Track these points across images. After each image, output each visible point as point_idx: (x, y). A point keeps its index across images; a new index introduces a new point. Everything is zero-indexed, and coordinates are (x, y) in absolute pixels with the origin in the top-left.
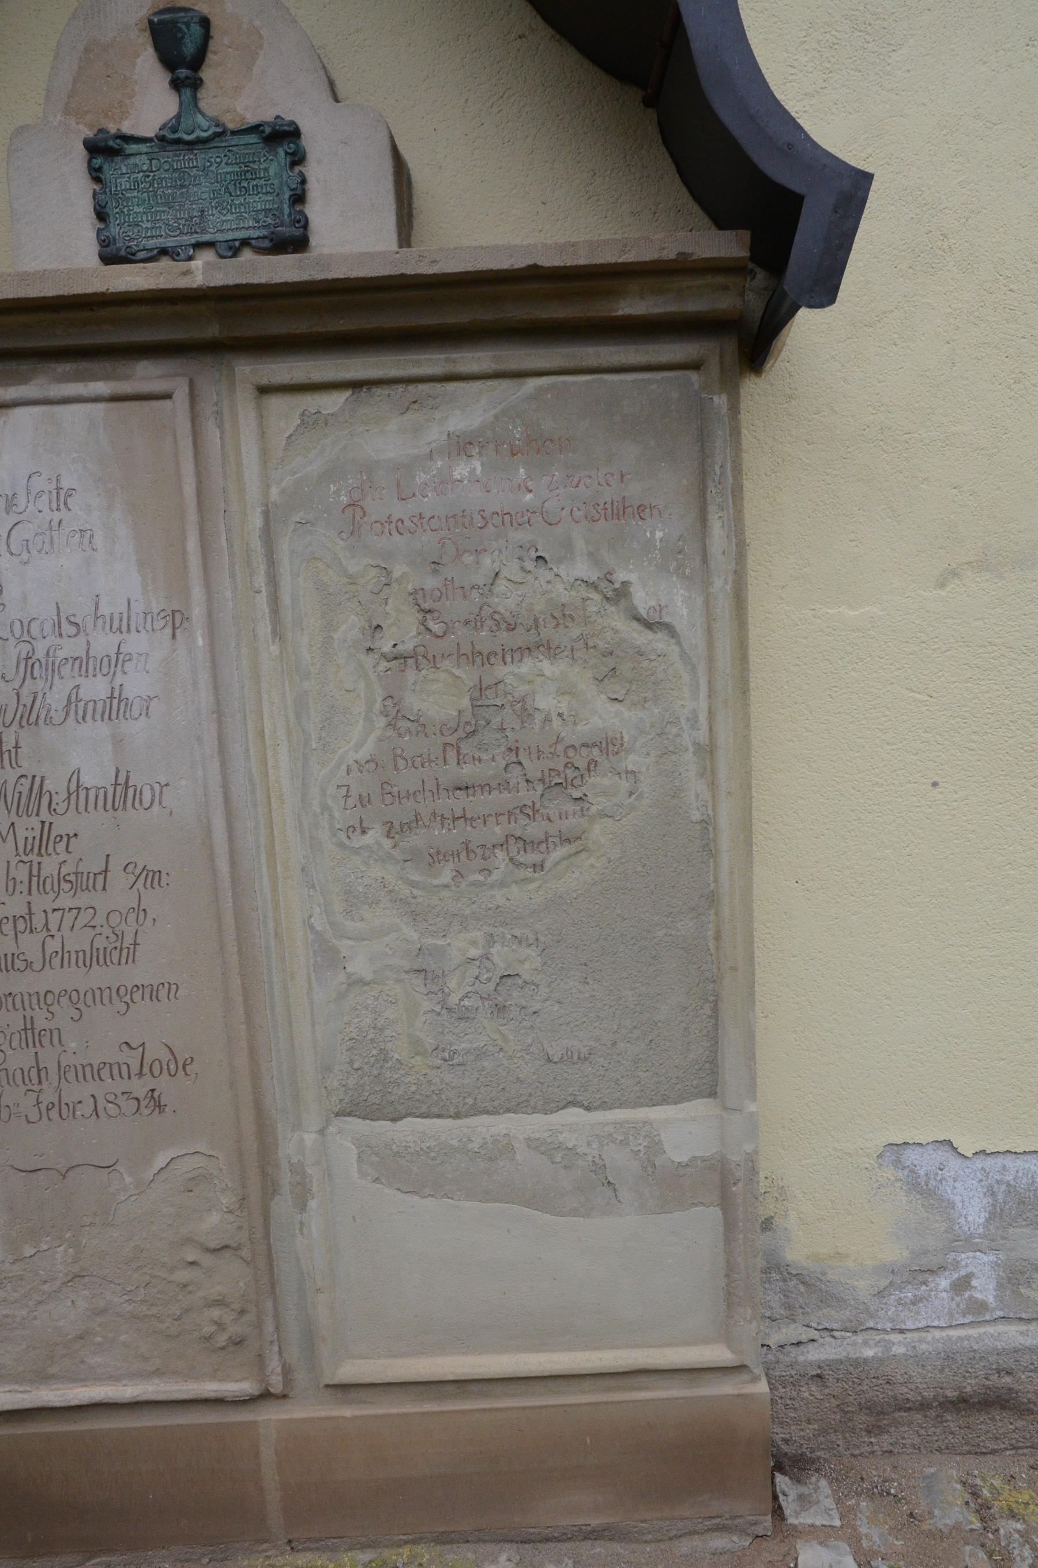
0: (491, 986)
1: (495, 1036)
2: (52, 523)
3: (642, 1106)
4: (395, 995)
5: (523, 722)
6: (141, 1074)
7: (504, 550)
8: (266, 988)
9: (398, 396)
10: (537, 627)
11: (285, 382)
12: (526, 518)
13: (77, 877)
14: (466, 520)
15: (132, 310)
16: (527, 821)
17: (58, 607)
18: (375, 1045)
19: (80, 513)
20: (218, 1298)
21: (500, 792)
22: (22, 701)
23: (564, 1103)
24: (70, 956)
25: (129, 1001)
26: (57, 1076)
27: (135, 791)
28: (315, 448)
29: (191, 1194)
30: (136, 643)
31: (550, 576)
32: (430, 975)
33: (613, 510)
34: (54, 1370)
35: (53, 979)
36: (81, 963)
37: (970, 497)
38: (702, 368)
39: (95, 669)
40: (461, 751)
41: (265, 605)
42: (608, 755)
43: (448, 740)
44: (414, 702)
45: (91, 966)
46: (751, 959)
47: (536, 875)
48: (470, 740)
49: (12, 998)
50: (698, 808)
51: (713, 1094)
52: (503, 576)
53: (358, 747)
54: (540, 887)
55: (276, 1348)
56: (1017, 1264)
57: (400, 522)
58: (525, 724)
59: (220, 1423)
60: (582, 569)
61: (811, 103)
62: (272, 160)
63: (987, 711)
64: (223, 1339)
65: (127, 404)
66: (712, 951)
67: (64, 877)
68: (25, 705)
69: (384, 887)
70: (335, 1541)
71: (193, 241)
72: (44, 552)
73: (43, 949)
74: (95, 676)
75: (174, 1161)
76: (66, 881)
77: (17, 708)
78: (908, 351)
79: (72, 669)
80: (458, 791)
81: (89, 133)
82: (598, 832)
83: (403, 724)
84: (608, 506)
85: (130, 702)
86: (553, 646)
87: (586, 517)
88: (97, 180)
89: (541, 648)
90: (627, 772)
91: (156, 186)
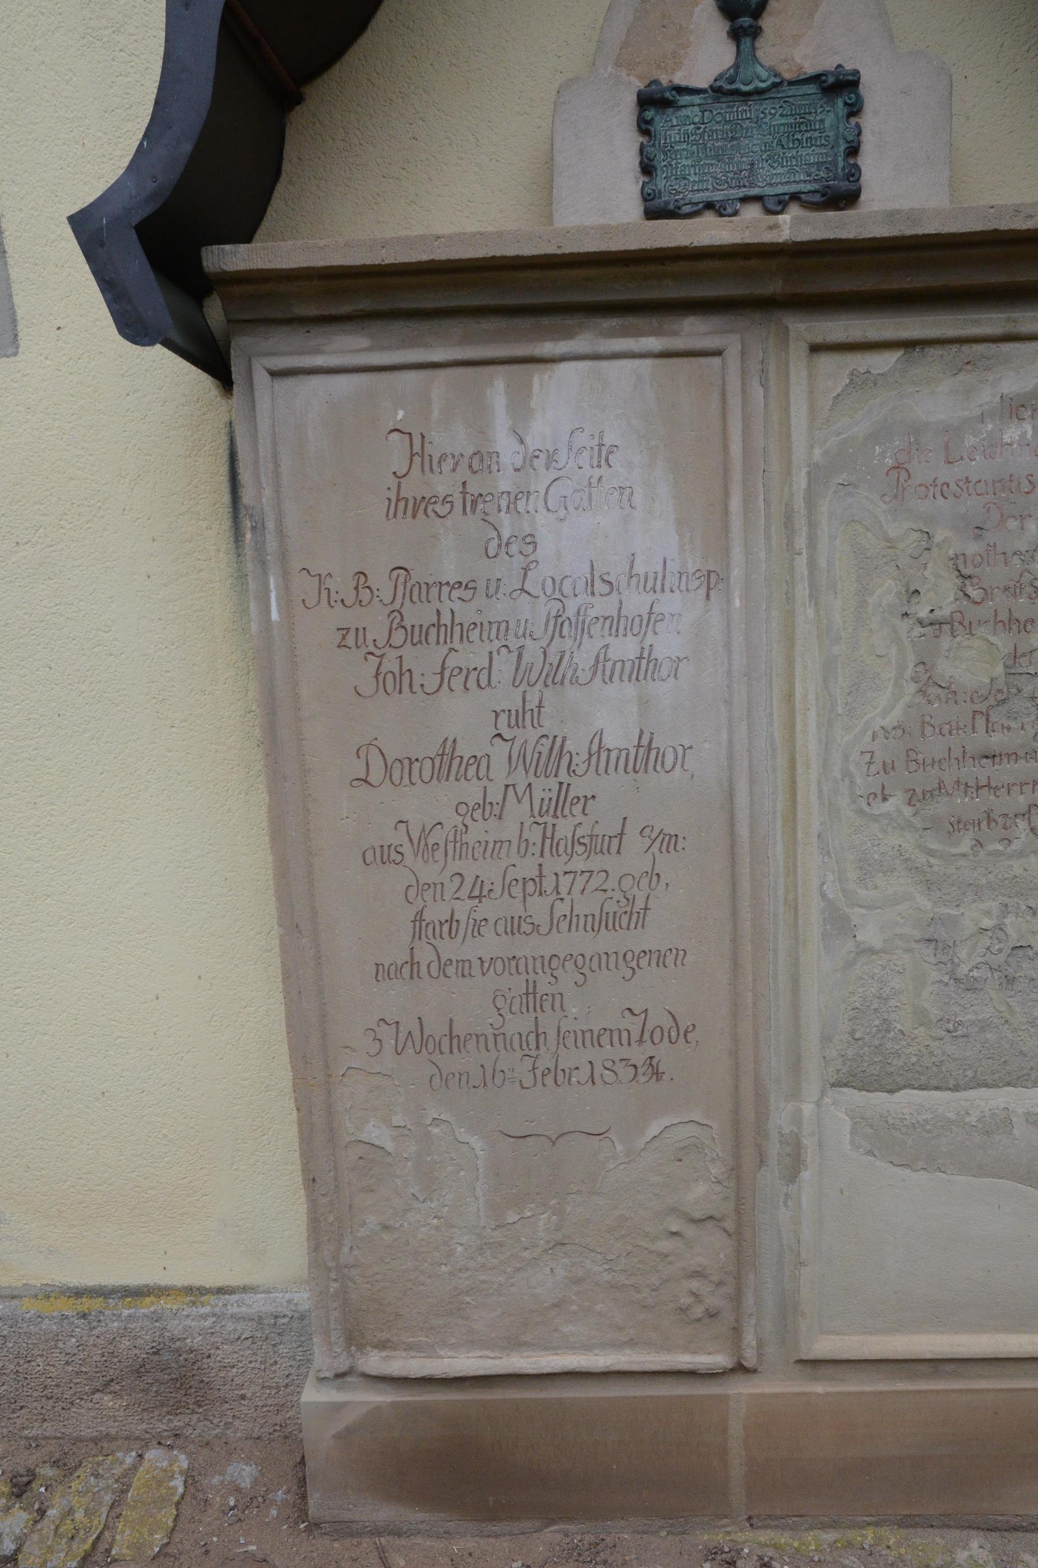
0: (1002, 958)
1: (1003, 1008)
2: (592, 480)
6: (641, 1041)
8: (771, 956)
13: (591, 840)
14: (1014, 485)
17: (592, 565)
18: (879, 1015)
20: (699, 1269)
24: (578, 920)
25: (635, 967)
27: (658, 753)
28: (862, 409)
30: (670, 603)
32: (940, 945)
34: (527, 1338)
35: (559, 943)
39: (626, 628)
40: (990, 719)
43: (977, 707)
44: (946, 669)
45: (599, 930)
48: (1000, 708)
49: (515, 962)
53: (885, 713)
55: (753, 1321)
57: (946, 486)
59: (691, 1396)
62: (828, 111)
64: (699, 1310)
67: (578, 839)
70: (796, 1519)
71: (741, 195)
73: (552, 913)
76: (580, 844)
77: (543, 666)
79: (603, 628)
81: (640, 84)
83: (933, 691)
91: (706, 138)
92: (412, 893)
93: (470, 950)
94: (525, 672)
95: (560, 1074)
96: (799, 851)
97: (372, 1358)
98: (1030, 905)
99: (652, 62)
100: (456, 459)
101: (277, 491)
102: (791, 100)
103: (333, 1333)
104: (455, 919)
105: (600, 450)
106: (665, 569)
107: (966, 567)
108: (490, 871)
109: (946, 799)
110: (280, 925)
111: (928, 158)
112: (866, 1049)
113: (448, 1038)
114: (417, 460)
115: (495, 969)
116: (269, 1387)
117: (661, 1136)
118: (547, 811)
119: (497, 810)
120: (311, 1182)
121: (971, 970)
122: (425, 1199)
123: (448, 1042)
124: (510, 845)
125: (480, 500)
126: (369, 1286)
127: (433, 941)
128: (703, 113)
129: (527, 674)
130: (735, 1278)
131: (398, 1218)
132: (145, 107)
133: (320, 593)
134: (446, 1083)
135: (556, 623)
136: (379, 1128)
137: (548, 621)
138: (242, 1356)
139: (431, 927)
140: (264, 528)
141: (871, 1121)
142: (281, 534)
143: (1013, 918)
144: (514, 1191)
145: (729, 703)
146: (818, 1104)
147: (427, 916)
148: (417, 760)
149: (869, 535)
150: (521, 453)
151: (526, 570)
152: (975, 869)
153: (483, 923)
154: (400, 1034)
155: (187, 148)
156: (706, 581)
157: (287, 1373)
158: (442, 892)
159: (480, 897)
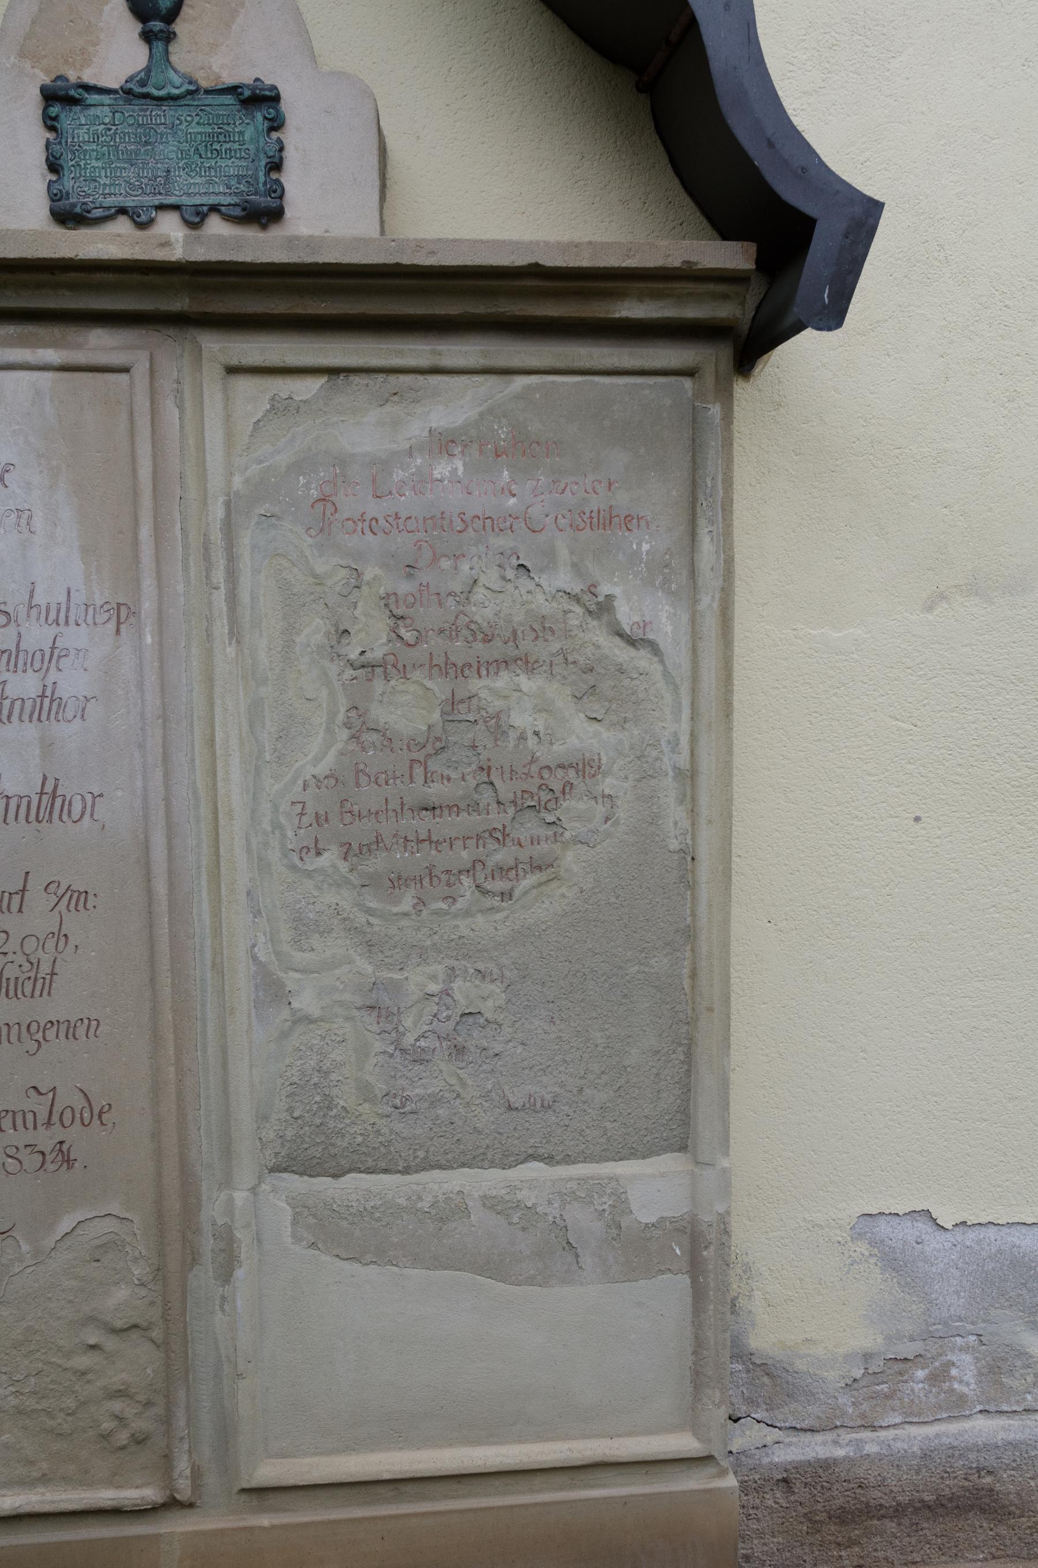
0: (451, 1024)
3: (607, 1160)
4: (344, 1034)
5: (496, 740)
6: (49, 1123)
7: (483, 556)
8: (199, 1027)
10: (515, 639)
12: (508, 524)
15: (98, 277)
16: (497, 846)
18: (319, 1090)
19: (18, 491)
21: (469, 814)
23: (522, 1157)
25: (41, 1040)
29: (99, 1264)
30: (74, 637)
31: (531, 586)
32: (383, 1012)
33: (599, 520)
37: (961, 518)
38: (696, 375)
39: (25, 664)
41: (224, 603)
42: (584, 777)
43: (415, 755)
44: (380, 714)
46: (727, 1000)
47: (504, 904)
48: (439, 757)
50: (676, 837)
51: (683, 1148)
52: (481, 584)
53: (316, 761)
54: (507, 918)
55: (186, 1446)
56: (999, 1350)
58: (499, 743)
60: (564, 579)
61: (809, 101)
62: (248, 124)
63: (973, 742)
64: (124, 1437)
66: (687, 990)
69: (338, 914)
71: (157, 203)
74: (25, 671)
75: (81, 1225)
78: (902, 363)
80: (424, 812)
82: (570, 859)
84: (595, 515)
85: (64, 702)
86: (531, 659)
87: (571, 525)
88: (52, 128)
89: (519, 662)
90: (604, 796)
91: (118, 140)
98: (479, 968)
102: (207, 108)
106: (69, 600)
107: (398, 608)
109: (384, 854)
111: (355, 180)
112: (307, 1128)
117: (75, 1233)
121: (417, 1040)
128: (114, 114)
130: (164, 1396)
141: (314, 1209)
143: (461, 983)
145: (141, 746)
146: (253, 1190)
149: (295, 570)
152: (419, 929)
156: (116, 614)
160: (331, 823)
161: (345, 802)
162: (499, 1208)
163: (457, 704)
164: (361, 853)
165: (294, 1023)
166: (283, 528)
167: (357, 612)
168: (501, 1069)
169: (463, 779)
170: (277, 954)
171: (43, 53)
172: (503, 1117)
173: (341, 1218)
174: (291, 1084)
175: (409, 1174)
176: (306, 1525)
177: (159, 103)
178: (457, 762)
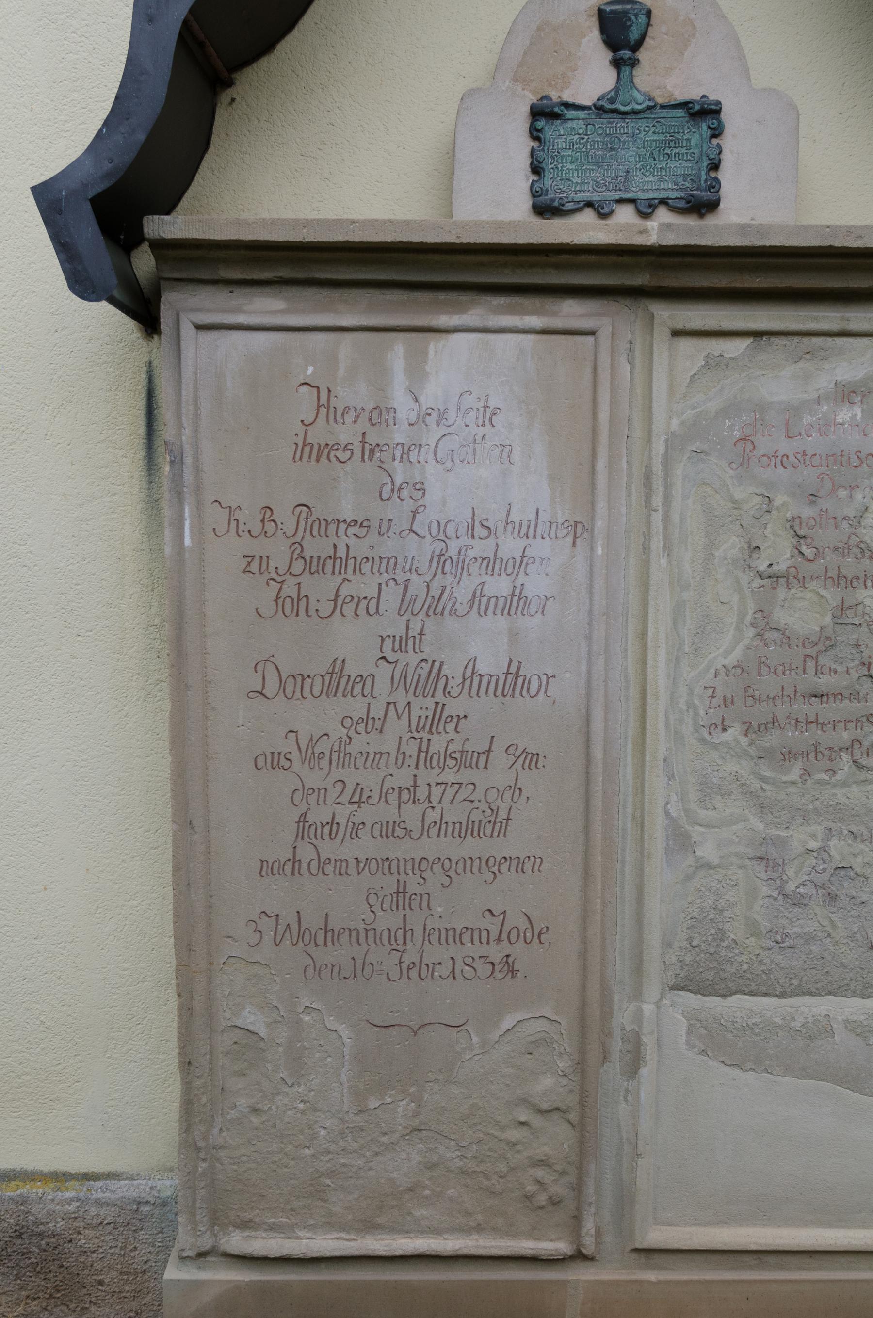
0: (826, 876)
1: (826, 923)
4: (737, 879)
6: (499, 940)
8: (619, 867)
9: (794, 346)
11: (697, 328)
13: (462, 756)
15: (583, 258)
17: (474, 512)
19: (502, 430)
20: (544, 1158)
22: (431, 593)
25: (497, 872)
26: (422, 938)
27: (524, 680)
30: (540, 548)
32: (771, 863)
34: (380, 1221)
36: (456, 834)
39: (501, 569)
41: (660, 523)
43: (808, 652)
44: (781, 617)
45: (465, 837)
53: (727, 653)
55: (593, 1210)
65: (553, 337)
67: (450, 754)
68: (433, 597)
69: (737, 780)
71: (617, 197)
72: (466, 462)
75: (520, 1024)
81: (533, 98)
91: (589, 147)
92: (298, 796)
93: (349, 850)
94: (410, 603)
95: (424, 967)
96: (647, 773)
97: (234, 1238)
98: (852, 830)
99: (545, 80)
100: (358, 411)
101: (196, 431)
103: (199, 1212)
104: (335, 822)
105: (485, 411)
107: (801, 529)
108: (370, 780)
109: (778, 732)
110: (173, 821)
113: (323, 931)
114: (323, 411)
115: (369, 868)
116: (127, 1274)
118: (424, 728)
119: (378, 724)
120: (186, 1066)
121: (797, 887)
122: (293, 1084)
123: (323, 935)
124: (389, 756)
125: (377, 449)
126: (235, 1167)
127: (314, 841)
128: (587, 126)
129: (412, 604)
131: (267, 1102)
132: (90, 80)
133: (229, 524)
134: (319, 974)
135: (439, 561)
136: (254, 1014)
137: (431, 561)
138: (103, 1241)
139: (313, 828)
140: (182, 463)
141: (706, 1023)
142: (197, 469)
144: (377, 1078)
146: (658, 1004)
147: (311, 818)
148: (309, 676)
149: (718, 497)
150: (415, 411)
151: (415, 513)
152: (803, 795)
153: (361, 827)
154: (279, 926)
155: (142, 137)
157: (145, 1259)
158: (325, 797)
159: (359, 803)
160: (735, 705)
161: (748, 688)
162: (859, 1031)
163: (846, 610)
164: (759, 731)
165: (697, 868)
166: (710, 462)
167: (767, 532)
168: (866, 915)
169: (848, 672)
170: (686, 811)
171: (532, 78)
172: (865, 955)
173: (727, 1031)
174: (692, 918)
175: (785, 998)
176: (678, 1282)
177: (624, 117)
178: (842, 658)
